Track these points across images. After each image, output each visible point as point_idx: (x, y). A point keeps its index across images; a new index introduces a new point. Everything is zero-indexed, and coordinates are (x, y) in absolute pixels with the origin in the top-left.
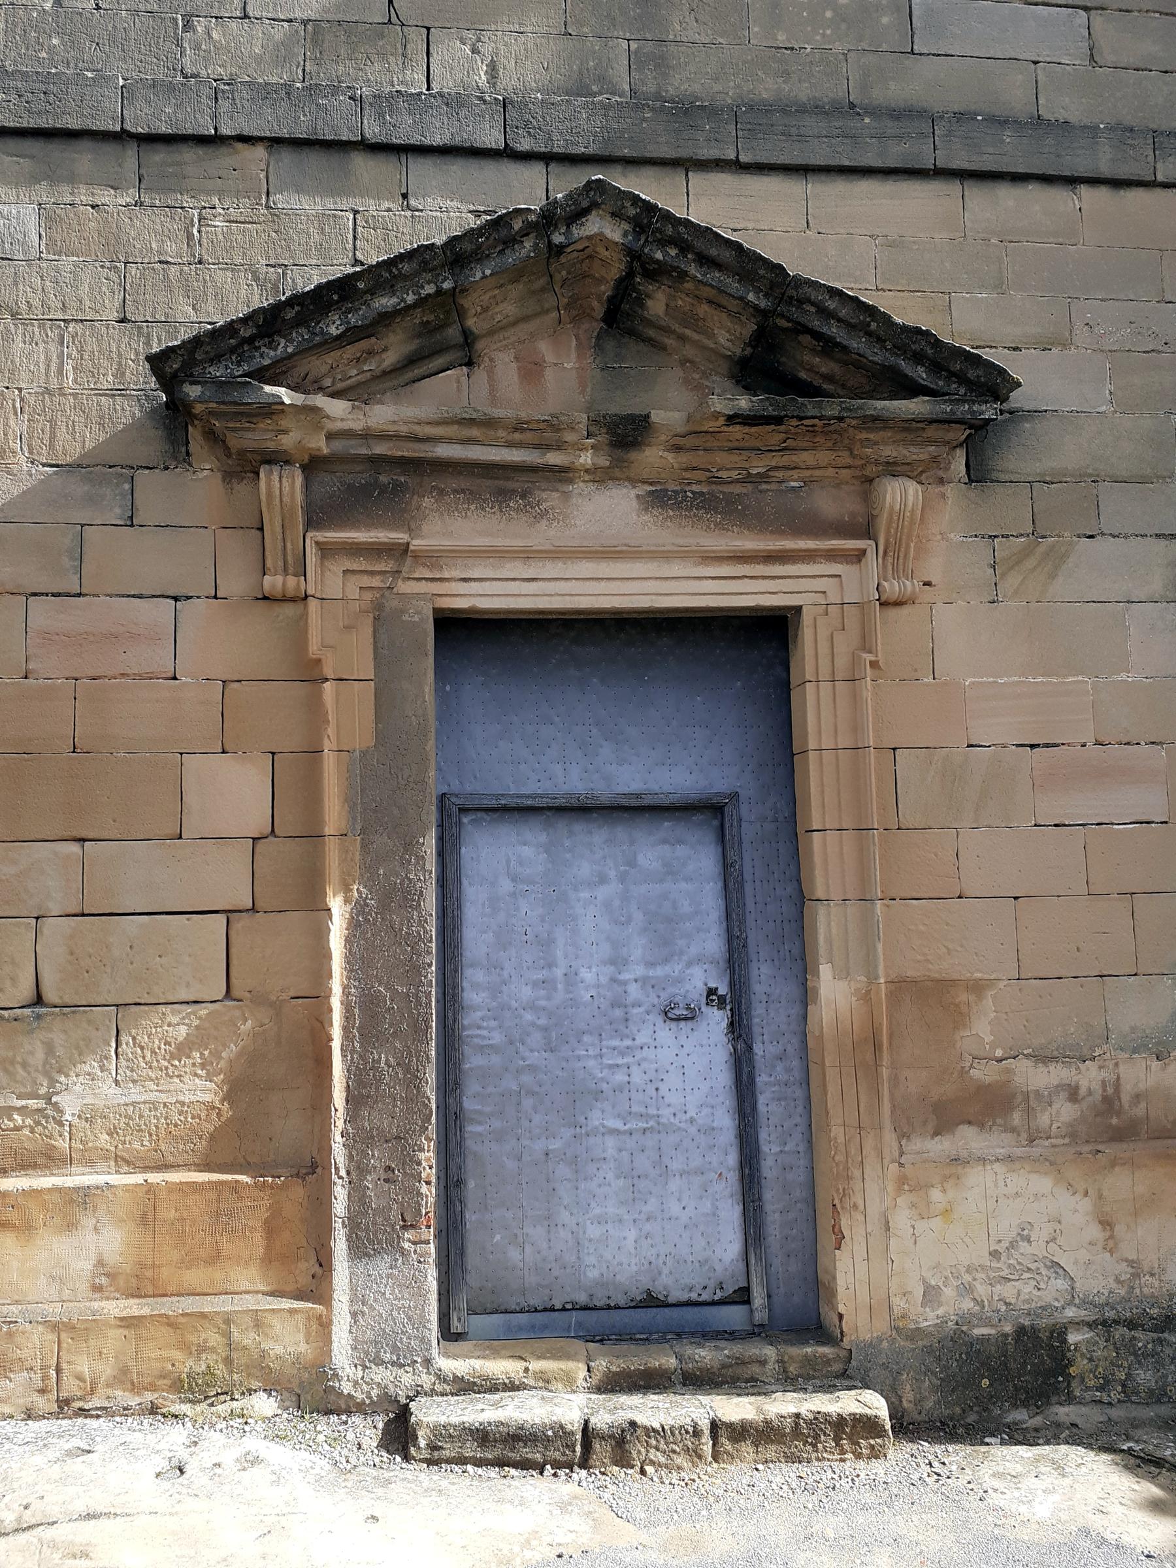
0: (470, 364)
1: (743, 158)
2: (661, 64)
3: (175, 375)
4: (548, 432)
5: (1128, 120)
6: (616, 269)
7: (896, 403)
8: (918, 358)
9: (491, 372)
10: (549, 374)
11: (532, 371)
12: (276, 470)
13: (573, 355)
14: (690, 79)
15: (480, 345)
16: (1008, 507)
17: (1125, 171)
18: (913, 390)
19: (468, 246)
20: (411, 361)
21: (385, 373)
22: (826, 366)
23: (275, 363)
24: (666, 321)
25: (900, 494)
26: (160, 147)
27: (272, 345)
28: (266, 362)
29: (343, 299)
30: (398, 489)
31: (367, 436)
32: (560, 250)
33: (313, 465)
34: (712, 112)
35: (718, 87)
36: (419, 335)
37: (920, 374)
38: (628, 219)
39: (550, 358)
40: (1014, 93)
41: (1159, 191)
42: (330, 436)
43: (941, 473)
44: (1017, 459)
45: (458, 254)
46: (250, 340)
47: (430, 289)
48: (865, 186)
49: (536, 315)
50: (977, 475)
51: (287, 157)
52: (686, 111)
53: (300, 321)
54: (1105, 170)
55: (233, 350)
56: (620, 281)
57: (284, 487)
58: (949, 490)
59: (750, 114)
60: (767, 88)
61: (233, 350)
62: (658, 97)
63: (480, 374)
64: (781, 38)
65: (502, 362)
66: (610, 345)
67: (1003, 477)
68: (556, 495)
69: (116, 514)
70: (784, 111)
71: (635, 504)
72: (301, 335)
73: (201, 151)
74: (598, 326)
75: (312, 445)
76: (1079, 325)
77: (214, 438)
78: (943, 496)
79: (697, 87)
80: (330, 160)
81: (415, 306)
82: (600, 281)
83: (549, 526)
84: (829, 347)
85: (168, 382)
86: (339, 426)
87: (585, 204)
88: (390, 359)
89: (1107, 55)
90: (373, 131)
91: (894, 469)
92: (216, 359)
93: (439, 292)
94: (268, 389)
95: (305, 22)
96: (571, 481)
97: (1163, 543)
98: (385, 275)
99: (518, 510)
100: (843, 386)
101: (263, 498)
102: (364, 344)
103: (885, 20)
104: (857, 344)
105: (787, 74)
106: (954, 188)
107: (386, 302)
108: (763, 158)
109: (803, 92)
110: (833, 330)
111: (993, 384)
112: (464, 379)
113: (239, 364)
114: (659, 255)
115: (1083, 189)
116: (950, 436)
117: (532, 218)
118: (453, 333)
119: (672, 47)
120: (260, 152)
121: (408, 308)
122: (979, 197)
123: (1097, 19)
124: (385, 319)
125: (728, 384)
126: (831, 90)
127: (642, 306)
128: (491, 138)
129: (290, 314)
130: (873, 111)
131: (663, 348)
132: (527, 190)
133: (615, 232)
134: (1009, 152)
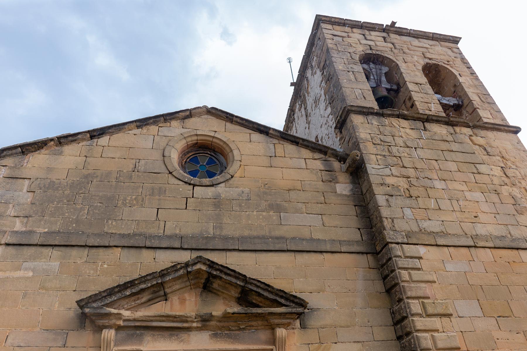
0: (166, 300)
1: (240, 249)
2: (221, 228)
3: (83, 306)
4: (183, 319)
5: (333, 238)
6: (205, 276)
7: (276, 309)
8: (282, 297)
9: (172, 302)
10: (187, 302)
11: (183, 301)
12: (107, 330)
13: (194, 297)
14: (228, 231)
15: (168, 296)
16: (312, 335)
17: (333, 250)
18: (282, 305)
19: (165, 272)
20: (149, 300)
21: (142, 303)
22: (260, 299)
23: (111, 302)
24: (218, 288)
25: (281, 332)
26: (95, 249)
27: (110, 298)
28: (108, 302)
29: (131, 286)
30: (141, 335)
31: (135, 320)
32: (190, 272)
33: (119, 328)
34: (233, 238)
35: (234, 233)
36: (152, 293)
37: (283, 301)
38: (207, 265)
39: (188, 298)
40: (306, 233)
41: (343, 254)
42: (124, 321)
43: (293, 327)
44: (313, 322)
45: (163, 273)
46: (105, 297)
47: (155, 283)
48: (270, 254)
49: (184, 288)
50: (303, 327)
51: (126, 250)
52: (226, 239)
53: (119, 291)
54: (329, 249)
55: (100, 299)
56: (206, 279)
57: (109, 334)
58: (295, 331)
59: (242, 239)
60: (246, 233)
61: (100, 299)
62: (220, 235)
63: (169, 303)
64: (250, 222)
65: (175, 299)
66: (204, 295)
67: (310, 327)
68: (186, 335)
69: (60, 344)
70: (250, 238)
71: (208, 337)
72: (119, 295)
73: (104, 249)
74: (201, 290)
75: (118, 323)
76: (327, 286)
77: (92, 322)
78: (294, 333)
79: (229, 233)
80: (138, 250)
81: (151, 287)
82: (202, 279)
83: (184, 344)
84: (259, 295)
85: (81, 307)
86: (127, 318)
87: (196, 261)
88: (143, 300)
89: (327, 224)
90: (148, 244)
91: (279, 325)
92: (94, 301)
93: (157, 283)
94: (108, 309)
95: (136, 221)
96: (191, 331)
97: (356, 344)
98: (143, 279)
99: (175, 340)
100: (265, 304)
101: (102, 339)
102: (137, 297)
103: (274, 218)
104: (266, 294)
105: (251, 230)
106: (293, 254)
107: (143, 286)
108: (245, 248)
109: (255, 233)
110: (259, 290)
111: (302, 303)
112: (164, 304)
113: (101, 303)
114: (215, 273)
115: (324, 254)
116: (293, 317)
117: (183, 265)
118: (162, 293)
119: (224, 225)
120: (120, 249)
121: (148, 287)
122: (299, 256)
123: (324, 217)
124: (143, 290)
125: (236, 304)
126: (261, 233)
127: (212, 285)
128: (177, 245)
129: (116, 290)
130: (271, 237)
131: (218, 295)
132: (185, 257)
133: (204, 268)
134: (305, 246)
